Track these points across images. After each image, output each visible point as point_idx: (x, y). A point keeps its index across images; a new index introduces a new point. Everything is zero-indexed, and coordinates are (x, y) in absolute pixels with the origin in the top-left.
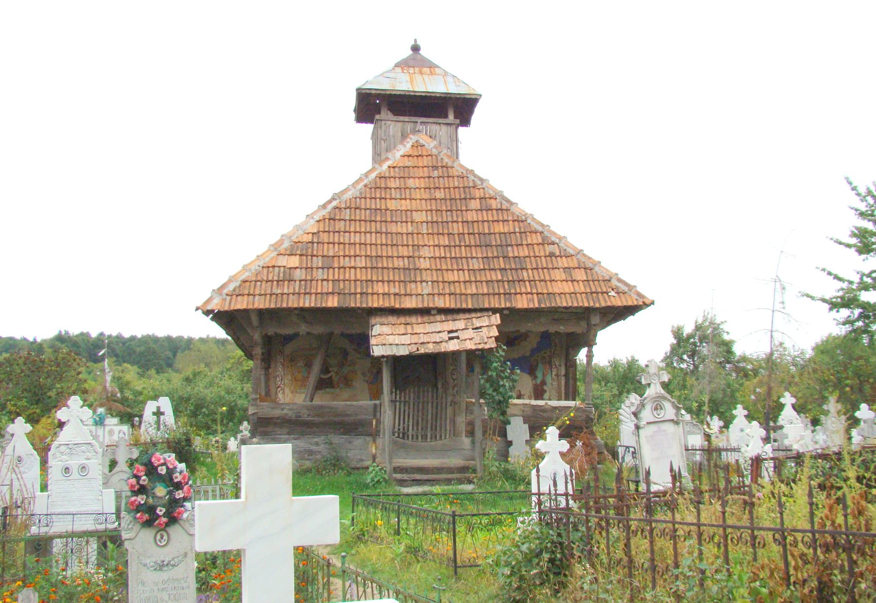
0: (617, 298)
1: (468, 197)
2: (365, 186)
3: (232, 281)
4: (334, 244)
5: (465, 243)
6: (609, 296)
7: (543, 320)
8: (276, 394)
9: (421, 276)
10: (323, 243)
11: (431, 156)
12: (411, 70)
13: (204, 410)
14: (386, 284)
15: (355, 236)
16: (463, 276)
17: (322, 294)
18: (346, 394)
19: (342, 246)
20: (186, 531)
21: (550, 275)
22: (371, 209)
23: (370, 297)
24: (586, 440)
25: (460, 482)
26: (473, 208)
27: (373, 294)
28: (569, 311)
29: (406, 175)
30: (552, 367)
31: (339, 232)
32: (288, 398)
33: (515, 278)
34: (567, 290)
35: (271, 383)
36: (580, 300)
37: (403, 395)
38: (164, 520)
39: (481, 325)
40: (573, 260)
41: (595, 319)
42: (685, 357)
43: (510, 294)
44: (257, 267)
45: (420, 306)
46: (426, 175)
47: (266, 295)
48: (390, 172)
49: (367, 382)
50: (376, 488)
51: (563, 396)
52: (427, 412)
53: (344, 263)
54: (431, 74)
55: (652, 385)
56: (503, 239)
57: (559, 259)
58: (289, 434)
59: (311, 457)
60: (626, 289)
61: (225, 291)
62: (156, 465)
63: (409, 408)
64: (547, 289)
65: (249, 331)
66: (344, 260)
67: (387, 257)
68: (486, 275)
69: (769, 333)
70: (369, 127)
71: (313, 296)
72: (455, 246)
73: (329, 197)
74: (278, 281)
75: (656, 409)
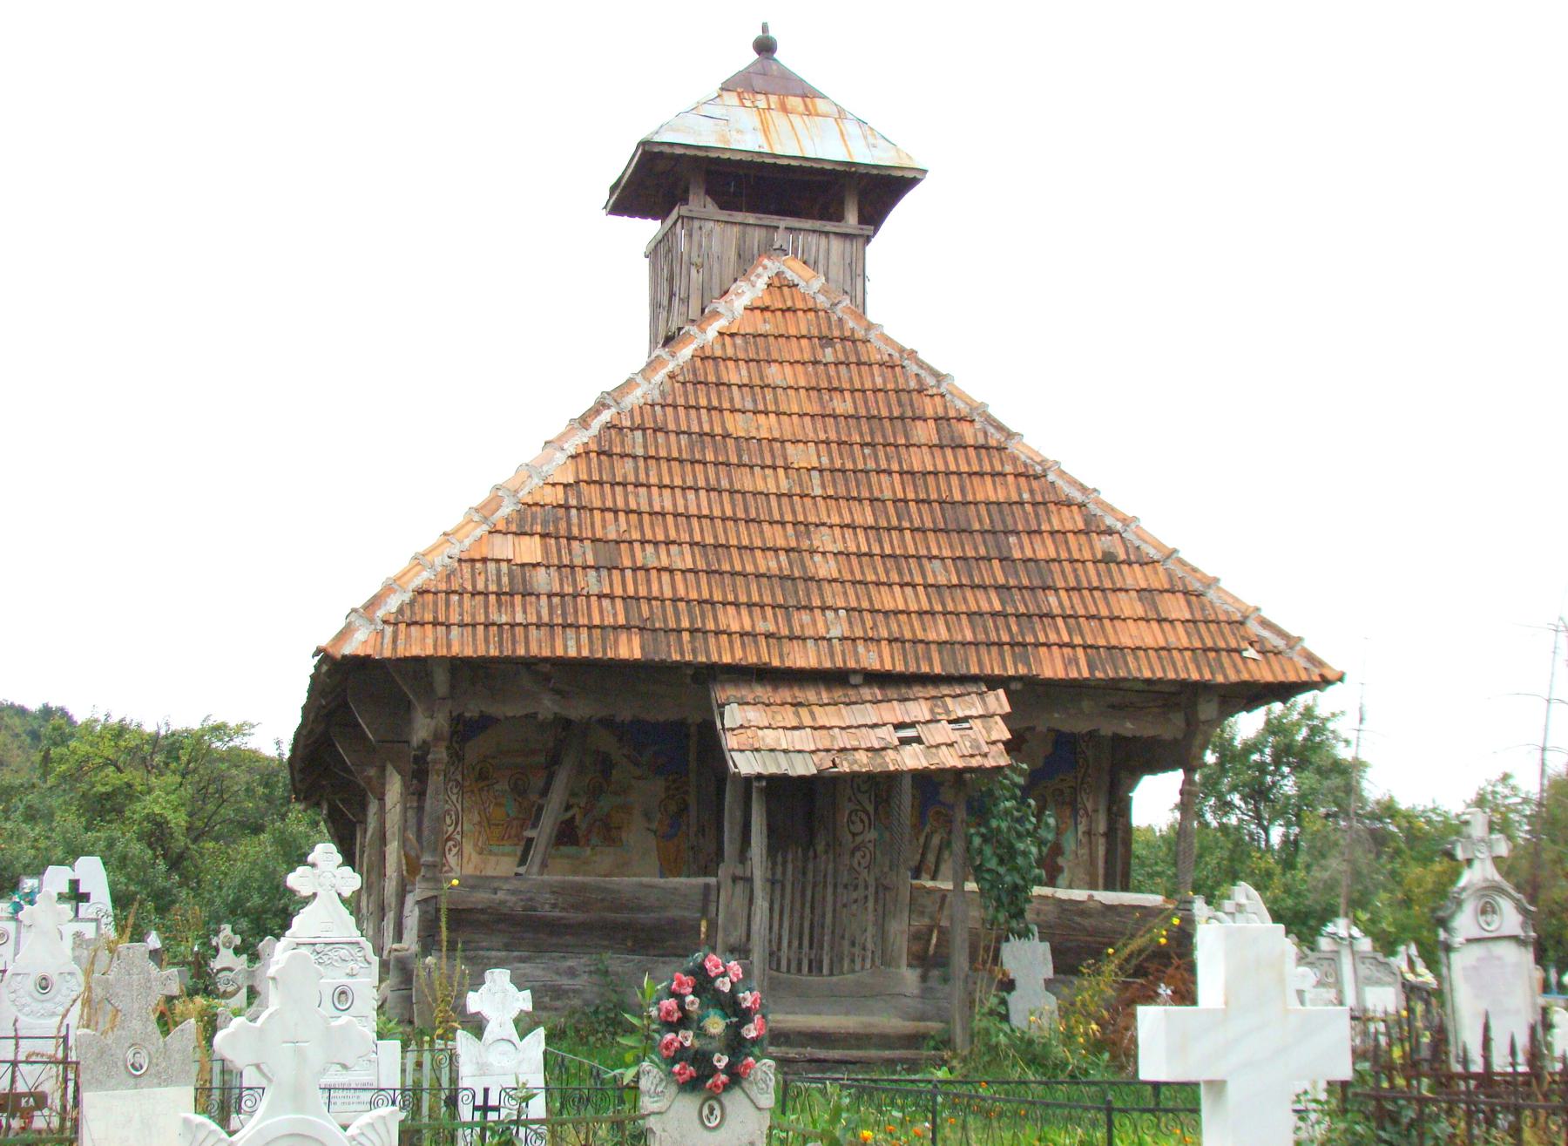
0: (1263, 664)
1: (909, 414)
2: (672, 376)
5: (911, 522)
6: (1244, 659)
7: (1086, 705)
9: (822, 597)
10: (592, 510)
11: (816, 311)
12: (761, 102)
14: (744, 611)
15: (661, 495)
16: (917, 600)
17: (602, 628)
18: (605, 859)
20: (752, 1101)
21: (1108, 604)
26: (923, 441)
27: (717, 633)
28: (1156, 688)
29: (762, 355)
31: (624, 485)
32: (471, 866)
33: (1033, 609)
34: (1150, 642)
36: (1180, 665)
38: (723, 1077)
39: (968, 713)
40: (1156, 573)
42: (1236, 798)
43: (1024, 645)
44: (448, 561)
45: (827, 664)
46: (807, 356)
47: (474, 626)
49: (655, 833)
51: (1101, 881)
53: (645, 558)
54: (809, 112)
55: (1476, 864)
56: (996, 517)
57: (1125, 567)
58: (508, 947)
59: (559, 1004)
60: (1280, 644)
62: (712, 974)
63: (783, 896)
64: (1106, 638)
66: (644, 550)
67: (739, 548)
68: (965, 599)
69: (1538, 755)
72: (888, 530)
73: (590, 403)
74: (498, 594)
75: (1484, 912)
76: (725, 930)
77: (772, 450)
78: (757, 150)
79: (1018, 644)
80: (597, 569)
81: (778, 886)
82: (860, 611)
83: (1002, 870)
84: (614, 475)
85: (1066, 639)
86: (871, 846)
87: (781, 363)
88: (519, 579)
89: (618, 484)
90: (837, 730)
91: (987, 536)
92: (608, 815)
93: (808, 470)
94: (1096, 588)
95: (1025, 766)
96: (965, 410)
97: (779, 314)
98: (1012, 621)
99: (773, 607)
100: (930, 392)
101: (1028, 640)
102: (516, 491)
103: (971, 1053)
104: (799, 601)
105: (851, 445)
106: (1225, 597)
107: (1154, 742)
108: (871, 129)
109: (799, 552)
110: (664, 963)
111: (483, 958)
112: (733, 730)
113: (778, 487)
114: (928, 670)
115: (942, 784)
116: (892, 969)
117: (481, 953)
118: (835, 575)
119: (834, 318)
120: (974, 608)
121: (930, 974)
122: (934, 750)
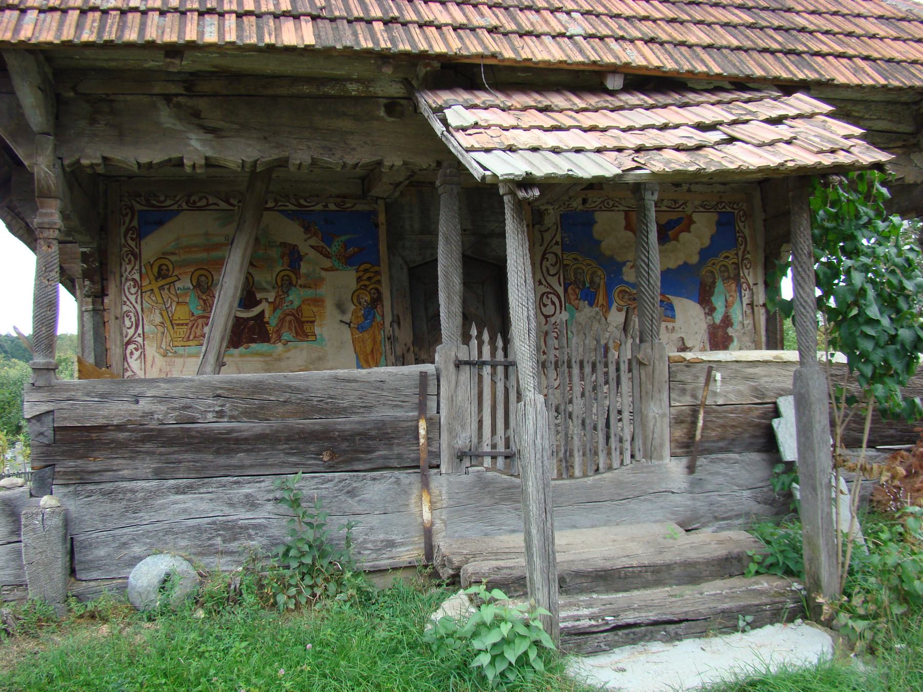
8: (125, 358)
18: (300, 352)
30: (741, 287)
47: (65, 11)
49: (349, 324)
51: (764, 346)
58: (159, 475)
59: (234, 546)
76: (451, 431)
92: (299, 309)
110: (374, 479)
111: (125, 491)
115: (624, 264)
116: (654, 462)
121: (698, 463)
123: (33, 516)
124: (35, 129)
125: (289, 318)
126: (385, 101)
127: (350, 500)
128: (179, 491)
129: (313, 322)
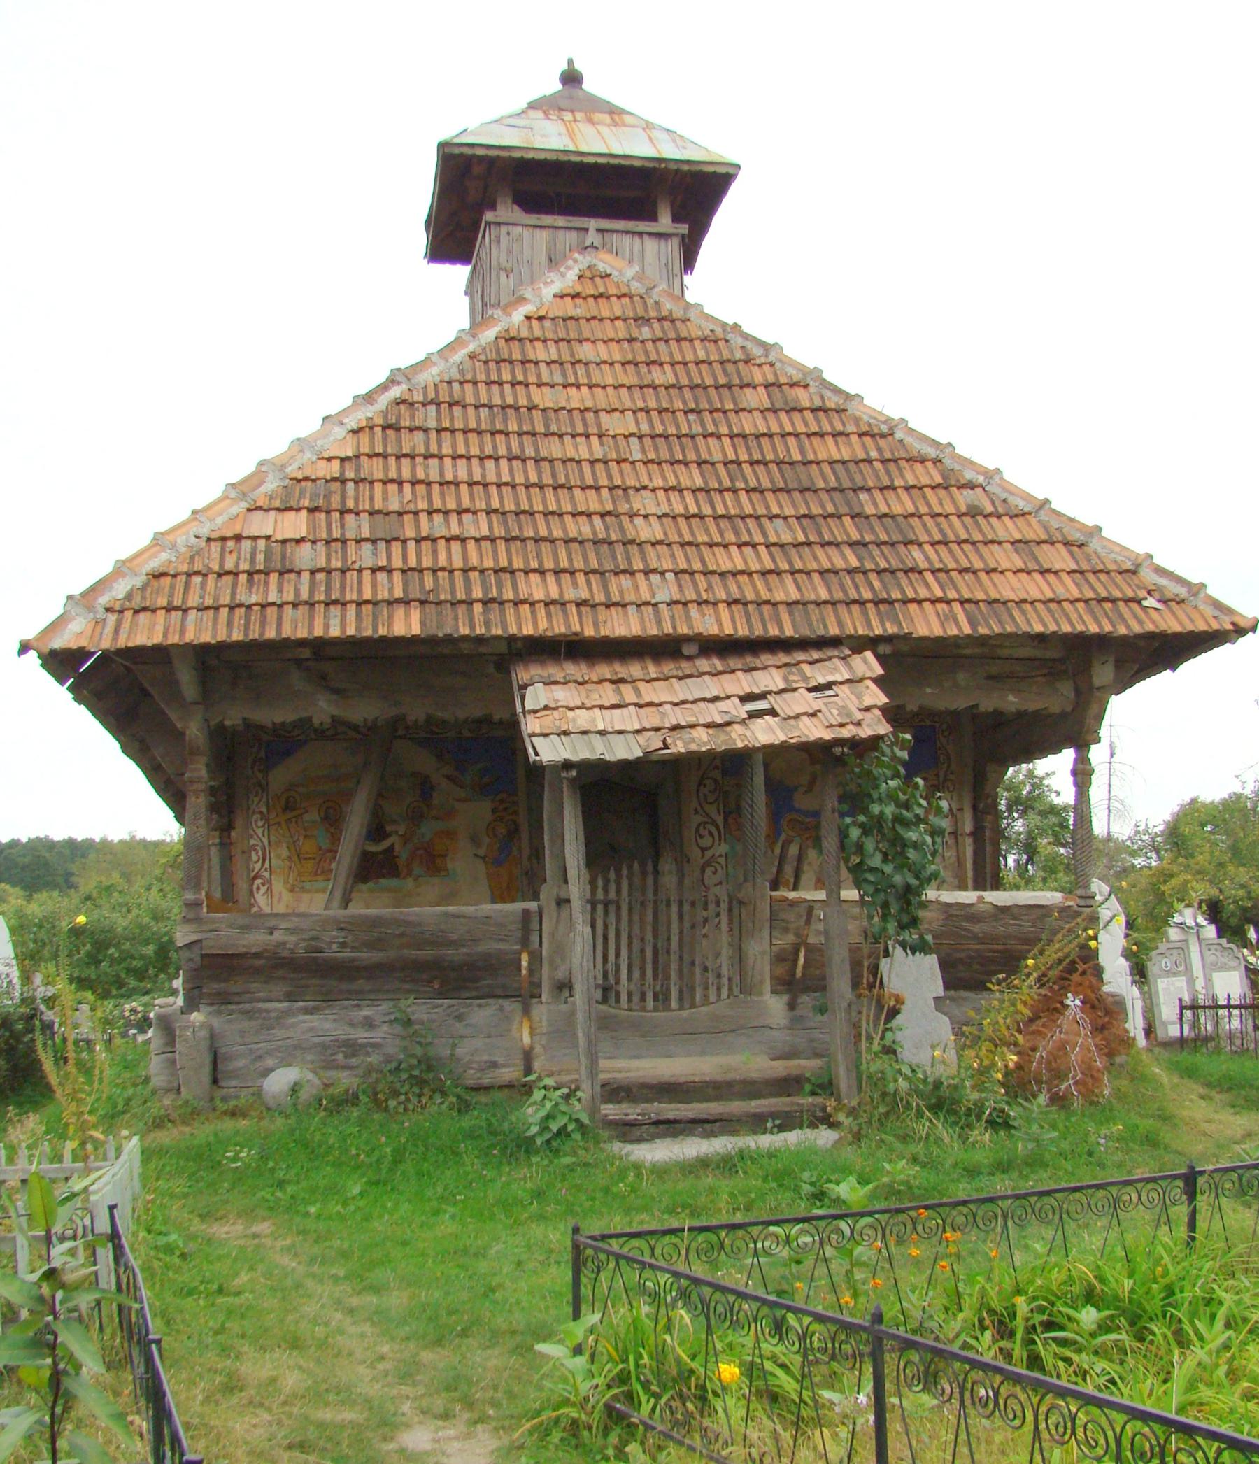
2: (472, 356)
3: (123, 575)
4: (400, 483)
5: (746, 482)
7: (961, 677)
9: (644, 559)
10: (371, 482)
12: (568, 116)
13: (112, 951)
14: (550, 579)
15: (454, 466)
17: (375, 603)
18: (432, 887)
19: (421, 489)
21: (981, 557)
22: (491, 407)
23: (510, 610)
24: (1089, 992)
25: (787, 1122)
26: (753, 406)
27: (517, 603)
31: (412, 457)
33: (895, 564)
35: (238, 865)
36: (1074, 617)
37: (600, 883)
39: (831, 678)
40: (1030, 525)
41: (1103, 673)
45: (653, 631)
47: (217, 608)
48: (531, 328)
49: (483, 858)
50: (556, 1152)
51: (970, 883)
52: (669, 931)
57: (993, 520)
58: (290, 997)
59: (354, 1061)
60: (1183, 592)
61: (103, 600)
65: (173, 715)
66: (431, 520)
67: (546, 514)
70: (461, 272)
71: (352, 609)
73: (381, 377)
74: (250, 574)
76: (551, 962)
77: (584, 420)
78: (562, 148)
79: (883, 601)
80: (374, 542)
81: (612, 908)
82: (692, 574)
83: (888, 869)
84: (401, 448)
85: (939, 593)
86: (722, 860)
87: (593, 342)
88: (277, 557)
89: (405, 456)
90: (668, 707)
91: (833, 494)
93: (626, 437)
94: (965, 541)
95: (908, 736)
96: (797, 376)
97: (591, 300)
98: (873, 577)
99: (586, 574)
100: (758, 362)
101: (894, 596)
102: (283, 467)
103: (859, 1104)
104: (617, 566)
105: (673, 412)
106: (1111, 546)
107: (1037, 717)
108: (681, 137)
109: (617, 516)
110: (480, 1006)
111: (261, 1011)
112: (535, 712)
113: (591, 453)
114: (777, 633)
115: (796, 788)
117: (260, 1005)
118: (660, 536)
119: (650, 302)
120: (826, 565)
121: (800, 1000)
122: (792, 722)
123: (185, 1028)
124: (189, 700)
125: (421, 852)
126: (495, 658)
127: (457, 1024)
128: (307, 1011)
129: (446, 856)
